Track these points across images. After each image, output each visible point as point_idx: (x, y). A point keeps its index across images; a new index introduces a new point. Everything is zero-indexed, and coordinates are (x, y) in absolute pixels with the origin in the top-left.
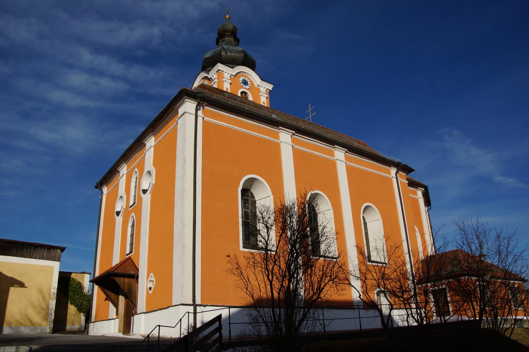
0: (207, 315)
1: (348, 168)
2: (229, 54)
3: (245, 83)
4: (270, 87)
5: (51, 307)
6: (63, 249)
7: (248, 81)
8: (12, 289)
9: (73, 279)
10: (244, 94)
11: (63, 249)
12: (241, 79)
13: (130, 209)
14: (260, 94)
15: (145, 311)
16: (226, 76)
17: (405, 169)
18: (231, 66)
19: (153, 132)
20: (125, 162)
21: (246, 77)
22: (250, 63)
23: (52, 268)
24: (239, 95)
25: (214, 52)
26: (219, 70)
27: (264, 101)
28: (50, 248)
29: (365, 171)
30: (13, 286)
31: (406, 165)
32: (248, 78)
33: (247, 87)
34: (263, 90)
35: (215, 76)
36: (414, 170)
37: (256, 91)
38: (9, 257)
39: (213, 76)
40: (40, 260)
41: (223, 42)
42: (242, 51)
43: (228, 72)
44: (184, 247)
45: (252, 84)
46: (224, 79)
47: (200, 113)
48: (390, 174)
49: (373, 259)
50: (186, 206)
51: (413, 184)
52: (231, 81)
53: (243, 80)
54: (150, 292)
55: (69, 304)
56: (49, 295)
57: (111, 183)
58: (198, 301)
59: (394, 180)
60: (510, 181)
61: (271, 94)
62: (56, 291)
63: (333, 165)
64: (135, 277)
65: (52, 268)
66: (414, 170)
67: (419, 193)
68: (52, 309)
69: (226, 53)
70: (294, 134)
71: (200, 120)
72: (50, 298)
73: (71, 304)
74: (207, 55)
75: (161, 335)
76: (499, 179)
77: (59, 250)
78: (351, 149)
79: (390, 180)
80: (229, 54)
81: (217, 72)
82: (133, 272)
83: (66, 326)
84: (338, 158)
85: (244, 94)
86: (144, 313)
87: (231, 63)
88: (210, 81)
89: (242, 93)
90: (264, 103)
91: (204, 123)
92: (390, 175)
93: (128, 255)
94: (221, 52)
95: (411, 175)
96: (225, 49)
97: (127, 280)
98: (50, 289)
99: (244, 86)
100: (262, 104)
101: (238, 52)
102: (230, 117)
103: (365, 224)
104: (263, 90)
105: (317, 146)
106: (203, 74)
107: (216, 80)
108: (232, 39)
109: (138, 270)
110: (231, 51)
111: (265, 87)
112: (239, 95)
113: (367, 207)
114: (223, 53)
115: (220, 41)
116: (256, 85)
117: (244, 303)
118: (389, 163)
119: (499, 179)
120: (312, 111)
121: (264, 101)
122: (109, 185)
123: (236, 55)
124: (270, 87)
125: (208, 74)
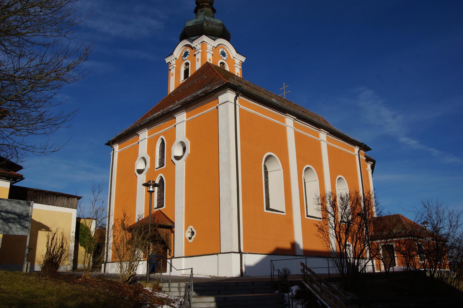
0: (252, 260)
1: (329, 147)
2: (210, 25)
3: (223, 54)
4: (243, 59)
5: (71, 249)
6: (79, 198)
7: (226, 52)
8: (40, 232)
9: (82, 224)
10: (222, 65)
11: (79, 198)
12: (220, 50)
13: (156, 170)
14: (235, 65)
15: (184, 256)
16: (209, 47)
17: (364, 147)
18: (213, 38)
19: (186, 109)
20: (147, 127)
21: (224, 49)
22: (225, 35)
23: (71, 214)
24: (219, 65)
25: (197, 22)
26: (203, 41)
27: (238, 71)
28: (69, 197)
29: (338, 149)
30: (41, 230)
31: (366, 145)
32: (226, 50)
33: (225, 58)
34: (237, 62)
35: (199, 47)
36: (371, 149)
37: (232, 62)
38: (63, 208)
39: (196, 46)
40: (61, 208)
41: (202, 11)
42: (221, 24)
43: (211, 44)
44: (232, 209)
45: (229, 56)
46: (207, 51)
47: (237, 101)
48: (354, 152)
49: (271, 207)
50: (232, 177)
51: (368, 159)
52: (213, 53)
53: (222, 52)
54: (190, 241)
55: (79, 246)
56: (69, 238)
57: (124, 143)
58: (242, 250)
59: (357, 157)
60: (413, 143)
61: (243, 65)
62: (74, 235)
63: (283, 130)
64: (171, 228)
65: (71, 214)
66: (371, 149)
67: (369, 166)
68: (72, 250)
69: (208, 25)
70: (295, 120)
71: (237, 107)
72: (70, 241)
73: (81, 245)
74: (189, 24)
75: (395, 270)
76: (404, 140)
77: (76, 199)
78: (332, 132)
79: (354, 156)
80: (210, 25)
81: (201, 43)
82: (170, 224)
83: (77, 265)
84: (323, 139)
85: (222, 65)
86: (184, 257)
87: (214, 35)
88: (192, 49)
89: (221, 63)
90: (238, 74)
91: (240, 109)
92: (285, 123)
93: (155, 208)
94: (203, 23)
95: (368, 153)
96: (207, 21)
97: (165, 230)
98: (70, 234)
99: (223, 57)
100: (236, 74)
101: (218, 24)
102: (255, 105)
103: (266, 173)
104: (237, 62)
105: (309, 129)
106: (185, 42)
107: (201, 51)
108: (210, 10)
109: (174, 224)
110: (212, 23)
111: (239, 59)
112: (219, 65)
113: (269, 157)
114: (205, 25)
115: (199, 10)
116: (232, 57)
117: (267, 252)
118: (354, 143)
119: (404, 140)
120: (287, 89)
121: (238, 71)
122: (122, 144)
123: (217, 27)
124: (243, 59)
125: (192, 43)
